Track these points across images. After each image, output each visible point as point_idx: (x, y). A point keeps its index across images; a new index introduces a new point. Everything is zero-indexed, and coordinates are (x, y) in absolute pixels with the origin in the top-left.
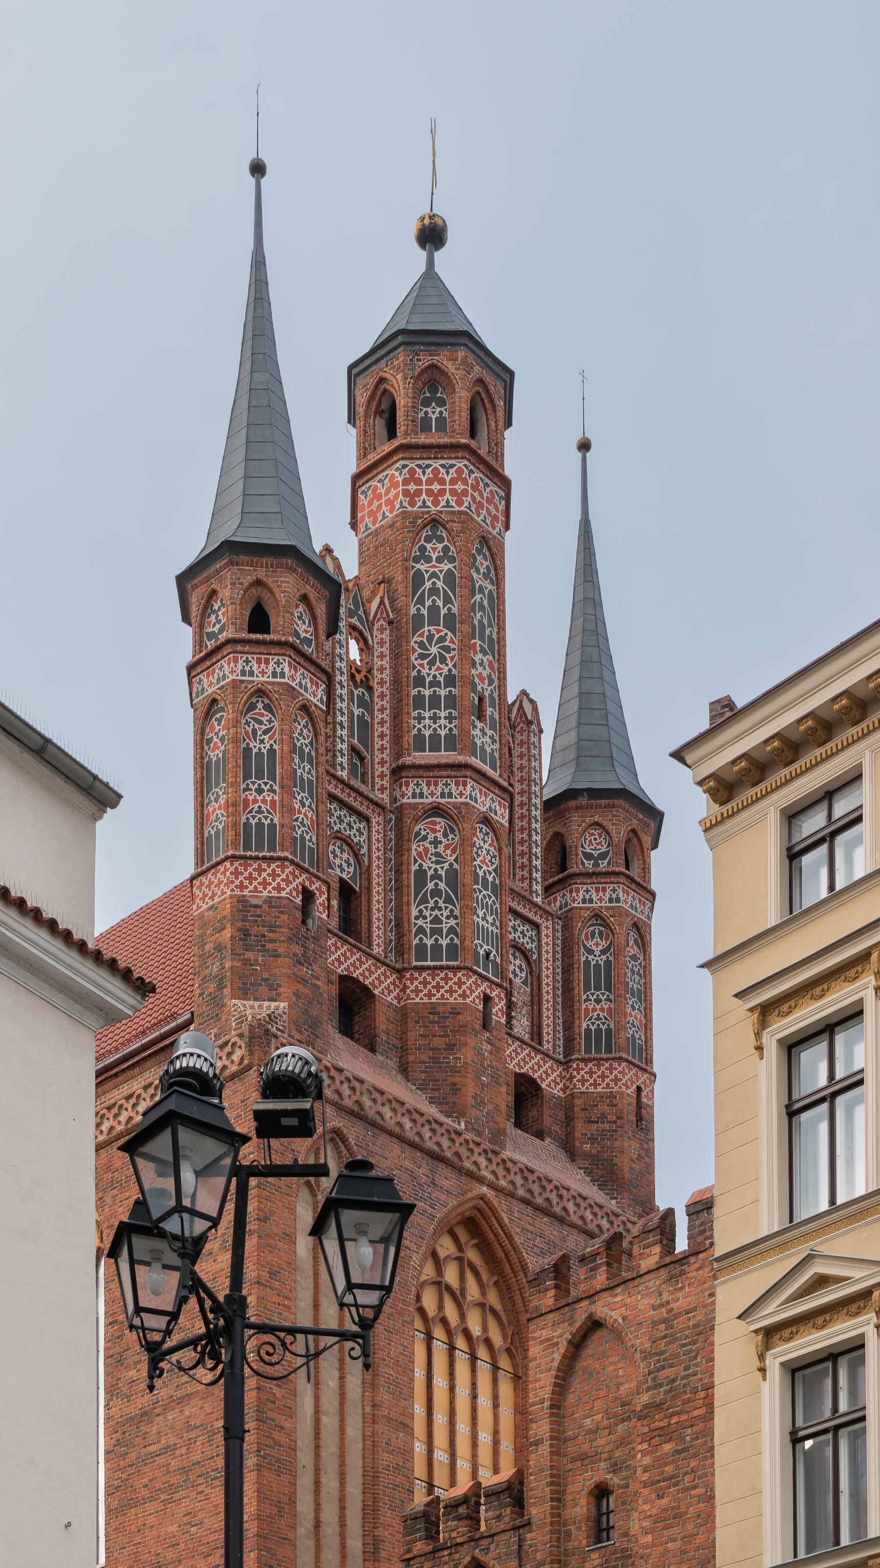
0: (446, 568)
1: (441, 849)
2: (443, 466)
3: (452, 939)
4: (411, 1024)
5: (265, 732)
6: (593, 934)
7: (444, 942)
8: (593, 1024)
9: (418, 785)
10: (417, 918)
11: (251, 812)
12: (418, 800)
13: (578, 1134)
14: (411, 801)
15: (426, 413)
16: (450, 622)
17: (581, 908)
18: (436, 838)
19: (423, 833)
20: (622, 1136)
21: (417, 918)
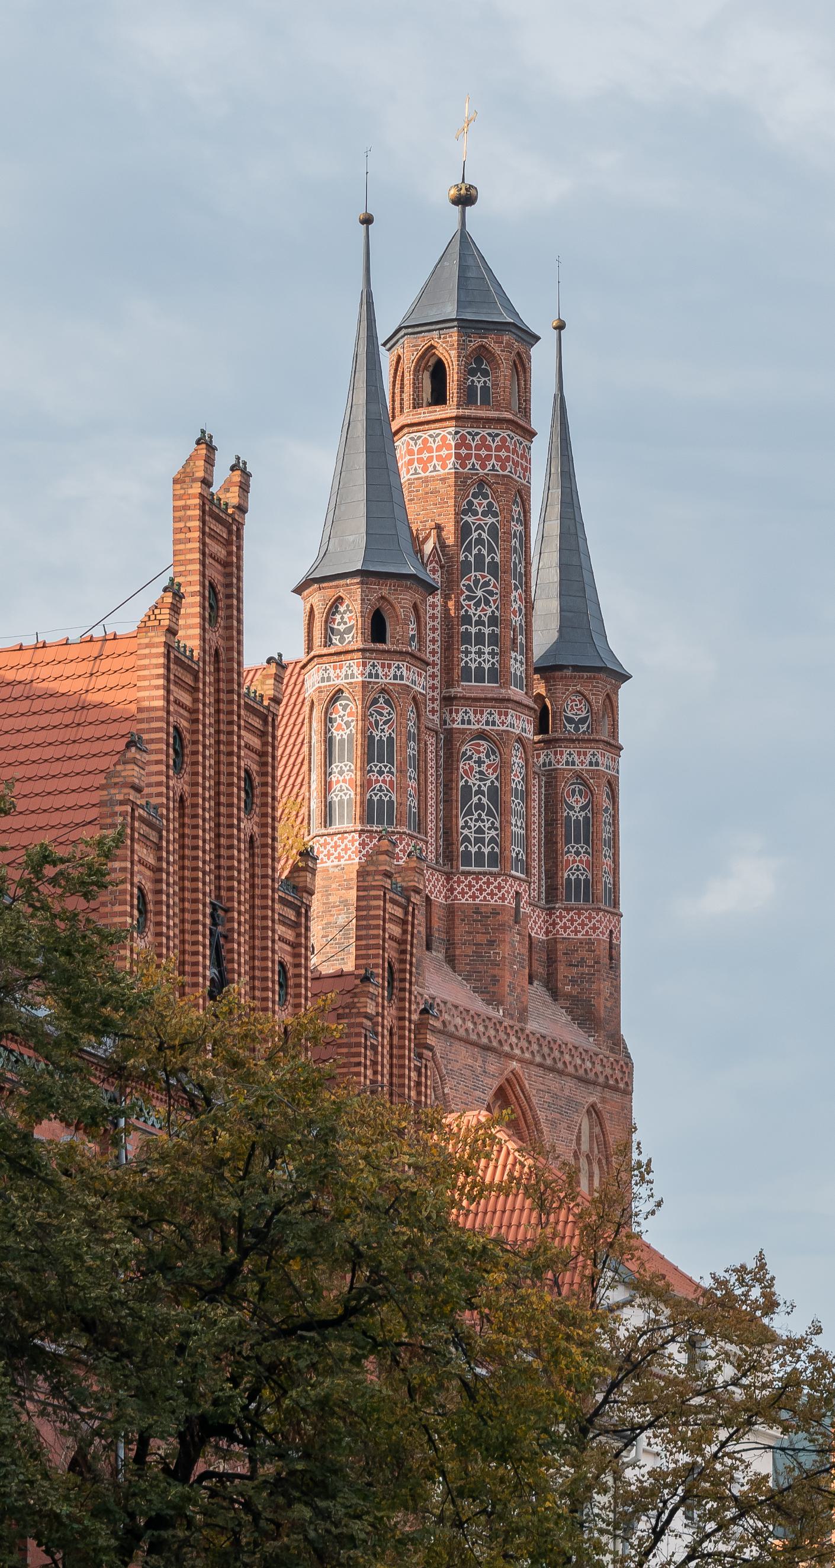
0: (490, 521)
1: (484, 768)
2: (489, 434)
3: (493, 848)
4: (457, 922)
5: (385, 723)
6: (574, 791)
7: (486, 850)
8: (573, 874)
9: (466, 712)
10: (463, 828)
11: (374, 790)
12: (466, 726)
13: (560, 977)
14: (461, 726)
15: (473, 381)
16: (494, 569)
17: (564, 770)
18: (479, 758)
19: (469, 753)
20: (599, 979)
21: (463, 828)
